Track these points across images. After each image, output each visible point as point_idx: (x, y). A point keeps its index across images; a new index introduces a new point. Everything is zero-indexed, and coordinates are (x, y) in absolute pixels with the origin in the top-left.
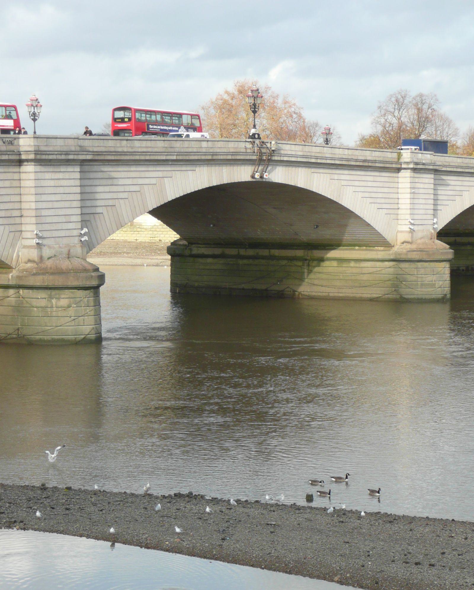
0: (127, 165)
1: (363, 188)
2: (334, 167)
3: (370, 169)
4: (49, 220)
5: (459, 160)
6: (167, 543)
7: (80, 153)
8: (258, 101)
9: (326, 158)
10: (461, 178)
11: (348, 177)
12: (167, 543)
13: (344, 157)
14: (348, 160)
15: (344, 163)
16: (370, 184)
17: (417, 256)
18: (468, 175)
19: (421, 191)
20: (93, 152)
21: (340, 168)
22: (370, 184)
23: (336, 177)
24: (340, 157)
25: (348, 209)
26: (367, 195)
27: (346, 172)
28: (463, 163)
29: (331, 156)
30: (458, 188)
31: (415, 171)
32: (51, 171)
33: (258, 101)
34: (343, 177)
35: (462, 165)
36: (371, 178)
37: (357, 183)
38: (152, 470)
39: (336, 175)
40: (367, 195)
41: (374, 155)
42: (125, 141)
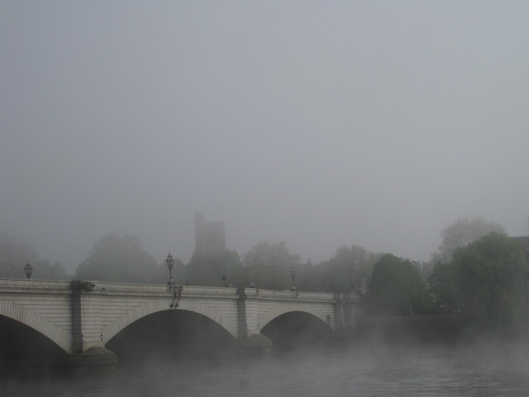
0: (12, 296)
5: (123, 287)
8: (172, 263)
9: (9, 288)
10: (125, 300)
11: (29, 302)
13: (25, 287)
14: (28, 289)
15: (24, 291)
16: (47, 307)
19: (91, 311)
20: (20, 288)
21: (21, 295)
22: (47, 307)
23: (18, 302)
24: (21, 287)
25: (198, 314)
27: (27, 298)
28: (126, 288)
29: (13, 286)
30: (123, 308)
33: (172, 263)
34: (24, 302)
36: (49, 303)
37: (36, 307)
42: (27, 282)
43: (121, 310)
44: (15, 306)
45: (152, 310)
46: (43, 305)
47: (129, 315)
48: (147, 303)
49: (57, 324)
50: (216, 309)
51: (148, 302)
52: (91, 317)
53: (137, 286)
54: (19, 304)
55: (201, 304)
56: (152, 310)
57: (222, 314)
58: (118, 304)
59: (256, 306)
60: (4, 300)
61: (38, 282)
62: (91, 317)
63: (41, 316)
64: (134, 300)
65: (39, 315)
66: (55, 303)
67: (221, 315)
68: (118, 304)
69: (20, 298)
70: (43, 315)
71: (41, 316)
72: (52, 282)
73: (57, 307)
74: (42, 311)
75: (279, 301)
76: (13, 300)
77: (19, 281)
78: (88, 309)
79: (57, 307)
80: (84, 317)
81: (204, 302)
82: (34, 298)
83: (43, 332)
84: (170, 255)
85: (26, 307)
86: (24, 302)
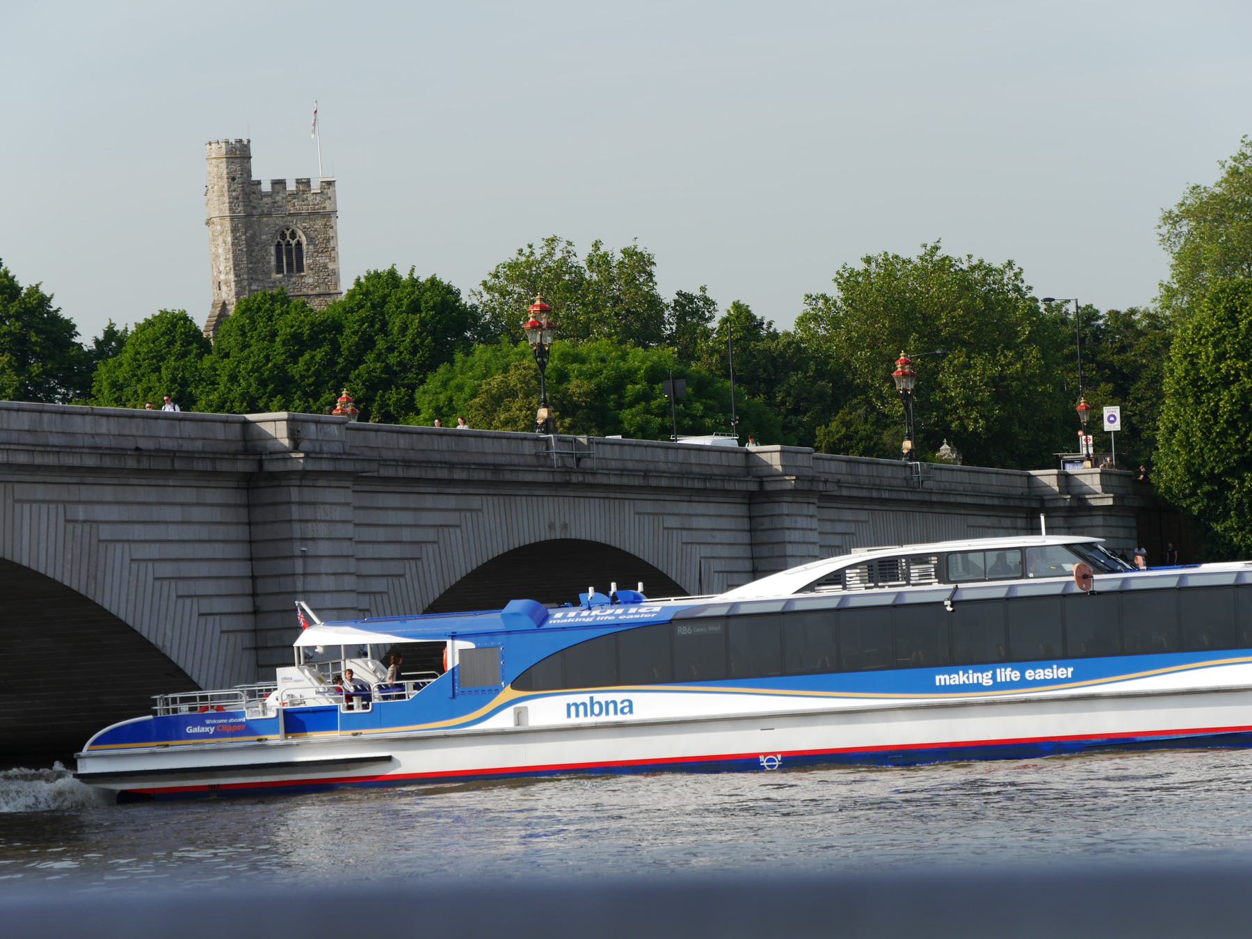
1: (155, 547)
2: (73, 480)
3: (171, 482)
4: (205, 569)
6: (1035, 319)
7: (540, 469)
11: (114, 513)
12: (1035, 319)
16: (173, 532)
17: (227, 808)
18: (429, 490)
22: (173, 532)
23: (81, 513)
26: (166, 570)
27: (108, 493)
28: (412, 449)
30: (407, 535)
31: (305, 482)
32: (109, 498)
34: (100, 513)
35: (412, 455)
36: (174, 513)
37: (138, 532)
38: (446, 840)
39: (81, 508)
40: (166, 570)
41: (178, 434)
43: (400, 542)
44: (70, 527)
45: (537, 533)
46: (158, 522)
47: (679, 539)
48: (480, 514)
49: (206, 606)
50: (686, 536)
51: (481, 510)
52: (326, 574)
53: (445, 438)
54: (85, 521)
55: (661, 517)
56: (537, 533)
57: (705, 558)
58: (393, 517)
59: (814, 524)
60: (35, 501)
61: (138, 420)
62: (326, 574)
63: (16, 498)
64: (442, 502)
65: (236, 637)
66: (197, 514)
67: (703, 561)
68: (393, 517)
69: (86, 493)
70: (141, 552)
71: (16, 498)
72: (182, 423)
73: (203, 532)
74: (154, 551)
75: (871, 500)
76: (64, 502)
77: (78, 419)
78: (313, 539)
79: (203, 532)
80: (304, 574)
81: (648, 507)
82: (128, 494)
83: (164, 646)
84: (603, 250)
85: (106, 532)
86: (100, 513)
